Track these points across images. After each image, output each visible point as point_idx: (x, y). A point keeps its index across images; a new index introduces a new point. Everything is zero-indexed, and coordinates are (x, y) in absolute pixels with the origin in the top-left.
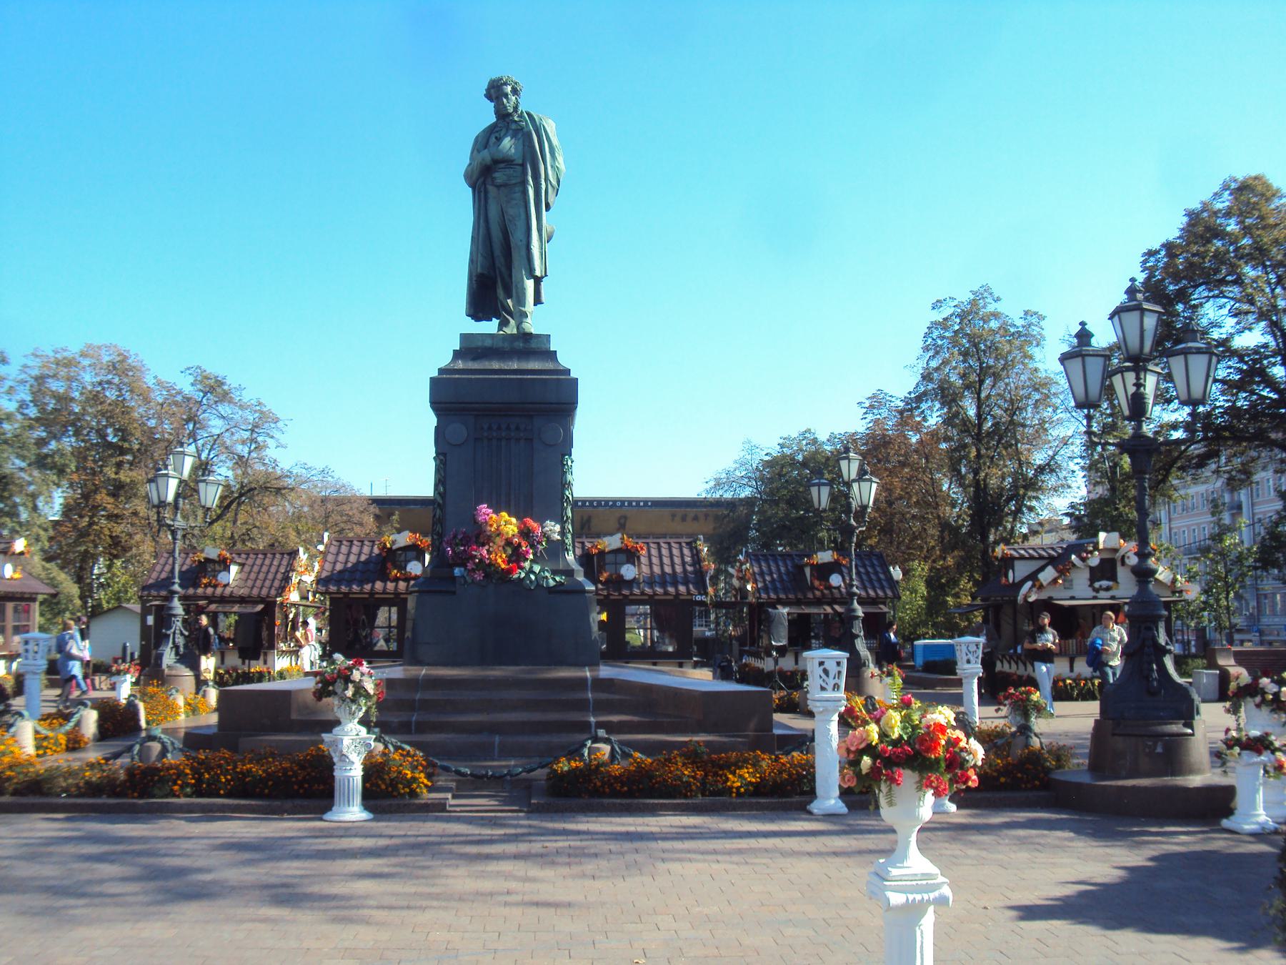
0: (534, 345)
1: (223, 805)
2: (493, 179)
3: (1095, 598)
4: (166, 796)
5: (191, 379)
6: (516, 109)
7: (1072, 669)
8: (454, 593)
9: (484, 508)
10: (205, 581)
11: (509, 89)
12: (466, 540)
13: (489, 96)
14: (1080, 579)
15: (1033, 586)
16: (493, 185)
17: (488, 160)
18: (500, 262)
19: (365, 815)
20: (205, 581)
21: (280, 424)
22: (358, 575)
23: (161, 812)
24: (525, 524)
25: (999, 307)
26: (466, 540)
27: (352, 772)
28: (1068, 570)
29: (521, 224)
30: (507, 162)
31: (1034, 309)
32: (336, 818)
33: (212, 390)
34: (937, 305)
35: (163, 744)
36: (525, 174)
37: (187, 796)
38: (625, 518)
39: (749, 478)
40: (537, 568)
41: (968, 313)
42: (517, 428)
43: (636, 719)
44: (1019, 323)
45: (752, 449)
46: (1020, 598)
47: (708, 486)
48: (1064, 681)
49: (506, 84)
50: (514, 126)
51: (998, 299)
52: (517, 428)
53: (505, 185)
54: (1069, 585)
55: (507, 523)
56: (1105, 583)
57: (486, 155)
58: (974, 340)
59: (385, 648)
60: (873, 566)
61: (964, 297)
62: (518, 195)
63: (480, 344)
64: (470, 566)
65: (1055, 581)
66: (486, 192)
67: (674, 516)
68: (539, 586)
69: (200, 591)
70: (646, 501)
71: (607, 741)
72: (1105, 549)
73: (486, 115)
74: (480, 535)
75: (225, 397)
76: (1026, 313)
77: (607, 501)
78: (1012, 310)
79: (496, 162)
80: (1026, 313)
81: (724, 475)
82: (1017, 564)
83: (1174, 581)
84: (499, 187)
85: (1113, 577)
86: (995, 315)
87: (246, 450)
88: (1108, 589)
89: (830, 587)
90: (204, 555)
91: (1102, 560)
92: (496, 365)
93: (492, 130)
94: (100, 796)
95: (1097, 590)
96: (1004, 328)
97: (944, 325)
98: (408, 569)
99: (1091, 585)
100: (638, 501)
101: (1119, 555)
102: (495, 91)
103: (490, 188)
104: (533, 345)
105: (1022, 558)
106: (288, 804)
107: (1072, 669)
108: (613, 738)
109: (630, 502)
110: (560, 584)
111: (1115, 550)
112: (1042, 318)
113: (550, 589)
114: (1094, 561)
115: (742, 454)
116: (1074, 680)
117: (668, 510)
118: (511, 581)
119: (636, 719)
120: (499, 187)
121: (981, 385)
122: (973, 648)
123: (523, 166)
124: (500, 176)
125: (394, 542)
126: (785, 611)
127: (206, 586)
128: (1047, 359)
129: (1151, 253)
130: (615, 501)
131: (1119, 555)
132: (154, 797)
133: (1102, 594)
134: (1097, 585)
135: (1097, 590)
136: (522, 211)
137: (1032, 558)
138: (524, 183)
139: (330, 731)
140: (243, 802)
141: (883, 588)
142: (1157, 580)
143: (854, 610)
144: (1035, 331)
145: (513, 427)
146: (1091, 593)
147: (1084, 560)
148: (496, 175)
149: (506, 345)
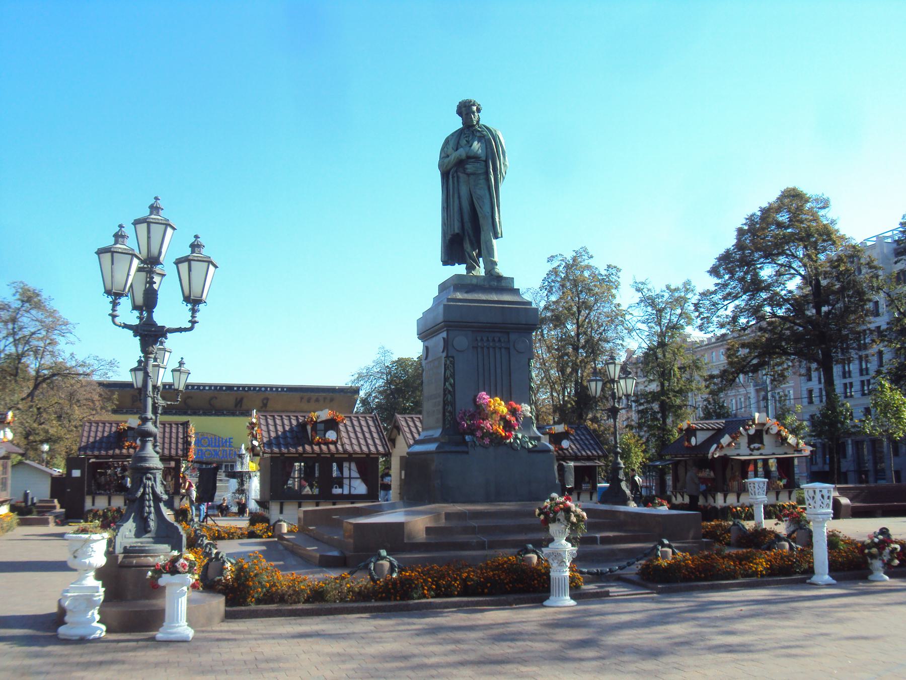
0: (503, 284)
1: (468, 602)
2: (465, 169)
3: (751, 455)
4: (419, 598)
5: (14, 291)
6: (478, 122)
7: (738, 501)
8: (467, 453)
9: (484, 395)
10: (127, 444)
11: (475, 108)
12: (472, 417)
13: (459, 113)
14: (743, 441)
15: (718, 447)
16: (464, 173)
17: (464, 156)
18: (468, 225)
19: (573, 603)
20: (127, 444)
21: (70, 327)
22: (104, 445)
23: (408, 610)
24: (511, 405)
25: (592, 262)
26: (472, 417)
27: (562, 573)
28: (737, 437)
29: (487, 201)
30: (475, 158)
31: (614, 265)
32: (560, 604)
33: (29, 300)
34: (551, 259)
35: (390, 562)
36: (487, 167)
37: (432, 597)
38: (267, 399)
39: (382, 373)
40: (520, 436)
41: (572, 265)
42: (500, 341)
43: (623, 534)
44: (604, 273)
45: (385, 352)
46: (710, 455)
47: (353, 378)
48: (736, 508)
49: (474, 105)
50: (478, 134)
51: (592, 257)
52: (500, 341)
53: (474, 174)
54: (738, 446)
55: (500, 404)
56: (757, 445)
57: (462, 153)
58: (575, 283)
59: (310, 493)
60: (583, 434)
61: (569, 256)
62: (482, 182)
63: (469, 282)
64: (479, 434)
65: (729, 445)
66: (458, 178)
67: (302, 398)
68: (523, 447)
69: (124, 451)
70: (283, 388)
71: (669, 546)
72: (759, 424)
73: (457, 123)
74: (480, 412)
75: (39, 306)
76: (609, 266)
77: (255, 387)
78: (600, 264)
79: (468, 157)
80: (609, 266)
81: (365, 371)
82: (698, 433)
83: (798, 444)
84: (468, 175)
85: (762, 442)
86: (588, 267)
87: (42, 345)
88: (759, 449)
89: (562, 449)
90: (127, 425)
91: (756, 431)
92: (494, 297)
93: (459, 134)
94: (370, 601)
95: (752, 450)
96: (594, 276)
97: (555, 271)
98: (327, 436)
99: (749, 447)
100: (277, 388)
101: (766, 427)
102: (466, 109)
103: (461, 175)
104: (503, 284)
105: (702, 429)
106: (511, 597)
107: (738, 501)
108: (673, 545)
109: (271, 387)
110: (535, 446)
111: (764, 424)
112: (618, 270)
113: (530, 451)
114: (752, 431)
115: (378, 356)
116: (741, 507)
117: (298, 395)
118: (505, 444)
119: (623, 534)
120: (468, 175)
121: (579, 315)
122: (761, 485)
123: (486, 162)
124: (470, 168)
125: (318, 417)
126: (572, 464)
127: (129, 447)
128: (625, 297)
129: (479, 110)
130: (260, 387)
131: (766, 427)
132: (413, 599)
133: (755, 452)
134: (752, 446)
135: (752, 450)
136: (487, 192)
137: (708, 429)
138: (487, 173)
139: (547, 546)
140: (470, 599)
141: (594, 449)
142: (788, 443)
143: (619, 464)
144: (613, 278)
145: (496, 339)
146: (748, 452)
147: (746, 430)
148: (468, 166)
149: (486, 283)
